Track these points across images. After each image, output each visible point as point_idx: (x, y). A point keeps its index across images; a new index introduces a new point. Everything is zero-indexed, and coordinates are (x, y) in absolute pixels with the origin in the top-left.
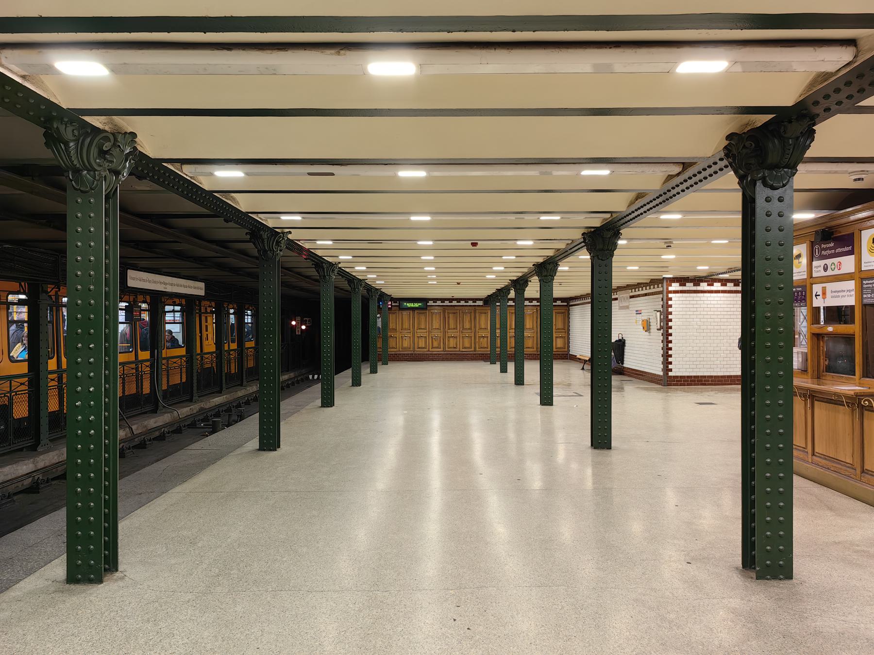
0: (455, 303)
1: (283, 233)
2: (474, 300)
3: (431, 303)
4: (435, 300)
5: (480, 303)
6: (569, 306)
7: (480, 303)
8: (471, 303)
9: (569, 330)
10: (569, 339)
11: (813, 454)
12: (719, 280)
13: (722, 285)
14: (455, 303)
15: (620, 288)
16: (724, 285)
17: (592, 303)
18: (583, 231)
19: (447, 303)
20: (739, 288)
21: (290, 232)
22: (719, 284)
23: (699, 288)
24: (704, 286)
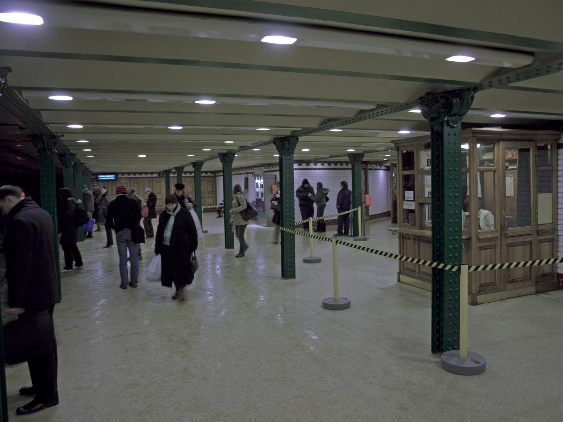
0: (137, 176)
1: (57, 136)
2: (152, 173)
3: (120, 176)
4: (123, 174)
5: (156, 175)
6: (215, 176)
7: (156, 175)
8: (149, 175)
9: (216, 192)
10: (216, 198)
11: (419, 273)
12: (320, 162)
13: (307, 165)
14: (137, 176)
15: (236, 169)
16: (323, 165)
17: (224, 176)
18: (274, 137)
19: (132, 176)
20: (176, 175)
21: (63, 136)
22: (305, 164)
23: (309, 167)
24: (312, 166)
